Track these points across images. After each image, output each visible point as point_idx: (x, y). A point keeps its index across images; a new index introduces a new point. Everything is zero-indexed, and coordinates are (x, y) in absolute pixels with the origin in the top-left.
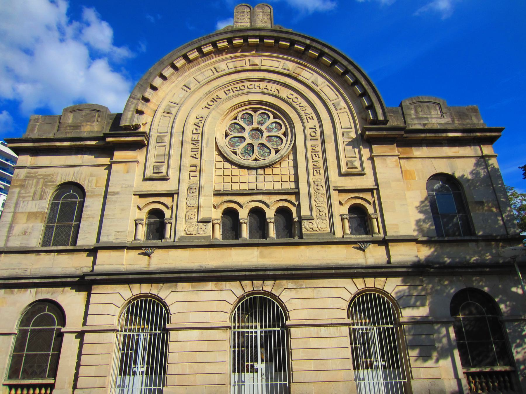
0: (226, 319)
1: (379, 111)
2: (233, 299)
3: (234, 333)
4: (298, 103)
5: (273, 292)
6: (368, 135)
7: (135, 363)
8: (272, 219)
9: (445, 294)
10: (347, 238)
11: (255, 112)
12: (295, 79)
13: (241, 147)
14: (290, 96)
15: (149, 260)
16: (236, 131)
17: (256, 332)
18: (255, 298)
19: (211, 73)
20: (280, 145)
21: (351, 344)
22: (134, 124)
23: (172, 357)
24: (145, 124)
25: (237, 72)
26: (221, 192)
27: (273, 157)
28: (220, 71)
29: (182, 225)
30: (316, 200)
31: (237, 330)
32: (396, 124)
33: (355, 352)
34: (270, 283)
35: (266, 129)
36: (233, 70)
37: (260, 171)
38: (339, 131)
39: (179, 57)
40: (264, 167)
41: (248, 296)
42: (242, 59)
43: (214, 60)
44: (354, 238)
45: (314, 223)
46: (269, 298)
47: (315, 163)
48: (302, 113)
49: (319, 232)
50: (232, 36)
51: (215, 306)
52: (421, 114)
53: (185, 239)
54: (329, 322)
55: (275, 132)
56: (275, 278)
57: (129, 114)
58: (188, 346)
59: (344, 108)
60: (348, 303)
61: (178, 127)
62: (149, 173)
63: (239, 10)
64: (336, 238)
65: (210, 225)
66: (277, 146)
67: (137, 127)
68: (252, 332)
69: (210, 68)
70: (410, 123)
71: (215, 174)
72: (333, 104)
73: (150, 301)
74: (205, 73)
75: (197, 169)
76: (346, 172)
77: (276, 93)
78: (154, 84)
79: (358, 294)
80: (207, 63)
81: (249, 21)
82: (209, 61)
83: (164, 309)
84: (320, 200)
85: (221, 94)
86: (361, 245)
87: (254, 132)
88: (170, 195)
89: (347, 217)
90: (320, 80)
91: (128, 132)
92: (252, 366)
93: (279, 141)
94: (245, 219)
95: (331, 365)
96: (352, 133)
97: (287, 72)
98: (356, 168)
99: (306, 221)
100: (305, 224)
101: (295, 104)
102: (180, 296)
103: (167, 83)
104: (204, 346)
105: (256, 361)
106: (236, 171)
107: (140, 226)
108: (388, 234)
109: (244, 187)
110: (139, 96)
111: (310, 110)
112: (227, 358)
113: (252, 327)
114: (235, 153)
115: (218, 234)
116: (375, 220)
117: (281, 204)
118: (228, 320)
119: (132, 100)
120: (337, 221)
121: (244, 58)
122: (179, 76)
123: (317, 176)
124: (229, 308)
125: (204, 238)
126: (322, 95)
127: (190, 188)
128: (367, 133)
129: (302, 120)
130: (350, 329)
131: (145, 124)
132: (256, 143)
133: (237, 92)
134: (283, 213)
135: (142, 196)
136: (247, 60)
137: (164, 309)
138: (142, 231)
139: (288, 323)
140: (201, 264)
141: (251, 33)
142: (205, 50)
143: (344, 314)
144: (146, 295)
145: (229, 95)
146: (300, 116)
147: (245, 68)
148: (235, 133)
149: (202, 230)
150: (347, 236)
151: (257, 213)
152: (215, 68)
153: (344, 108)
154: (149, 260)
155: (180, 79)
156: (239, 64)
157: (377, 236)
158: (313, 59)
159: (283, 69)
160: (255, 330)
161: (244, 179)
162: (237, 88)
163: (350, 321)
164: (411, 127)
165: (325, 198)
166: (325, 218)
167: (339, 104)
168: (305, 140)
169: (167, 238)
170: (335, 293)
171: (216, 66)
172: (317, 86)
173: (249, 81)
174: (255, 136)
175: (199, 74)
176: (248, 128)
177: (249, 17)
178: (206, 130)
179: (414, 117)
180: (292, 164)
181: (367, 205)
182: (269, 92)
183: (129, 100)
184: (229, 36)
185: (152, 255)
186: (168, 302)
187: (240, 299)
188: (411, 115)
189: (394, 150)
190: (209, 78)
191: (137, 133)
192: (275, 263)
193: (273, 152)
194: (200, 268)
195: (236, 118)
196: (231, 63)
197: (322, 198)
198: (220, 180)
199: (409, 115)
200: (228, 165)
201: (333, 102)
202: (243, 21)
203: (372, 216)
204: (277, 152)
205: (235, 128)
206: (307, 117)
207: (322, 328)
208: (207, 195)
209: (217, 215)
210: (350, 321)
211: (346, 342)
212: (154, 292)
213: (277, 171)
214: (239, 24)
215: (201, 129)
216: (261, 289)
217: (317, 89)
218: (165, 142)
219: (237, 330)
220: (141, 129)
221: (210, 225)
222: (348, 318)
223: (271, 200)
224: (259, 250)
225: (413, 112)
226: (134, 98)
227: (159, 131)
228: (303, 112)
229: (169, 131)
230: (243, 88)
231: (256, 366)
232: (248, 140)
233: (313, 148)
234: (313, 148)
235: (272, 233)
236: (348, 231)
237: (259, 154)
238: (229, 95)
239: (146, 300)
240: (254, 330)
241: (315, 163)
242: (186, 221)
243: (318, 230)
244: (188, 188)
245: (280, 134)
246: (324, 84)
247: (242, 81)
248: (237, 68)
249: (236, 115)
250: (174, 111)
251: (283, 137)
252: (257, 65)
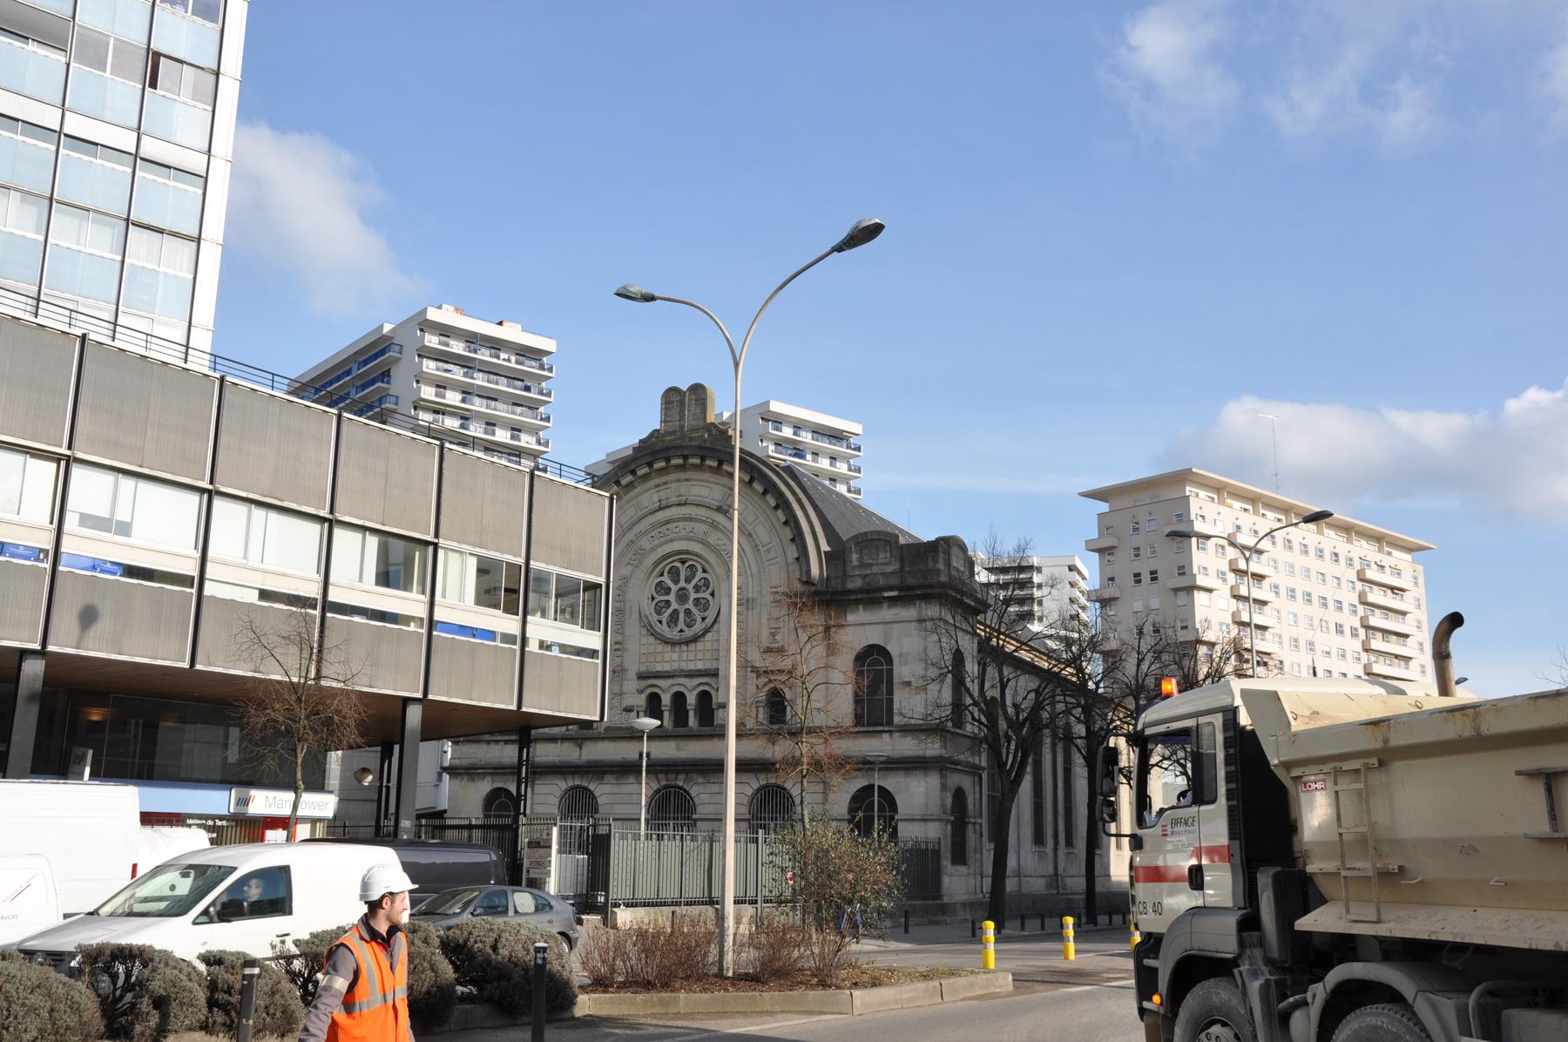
9: (1137, 938)
25: (661, 509)
52: (867, 560)
85: (645, 543)
106: (660, 648)
109: (667, 667)
117: (702, 688)
142: (624, 482)
151: (679, 698)
161: (667, 657)
184: (648, 459)
186: (597, 793)
213: (700, 645)
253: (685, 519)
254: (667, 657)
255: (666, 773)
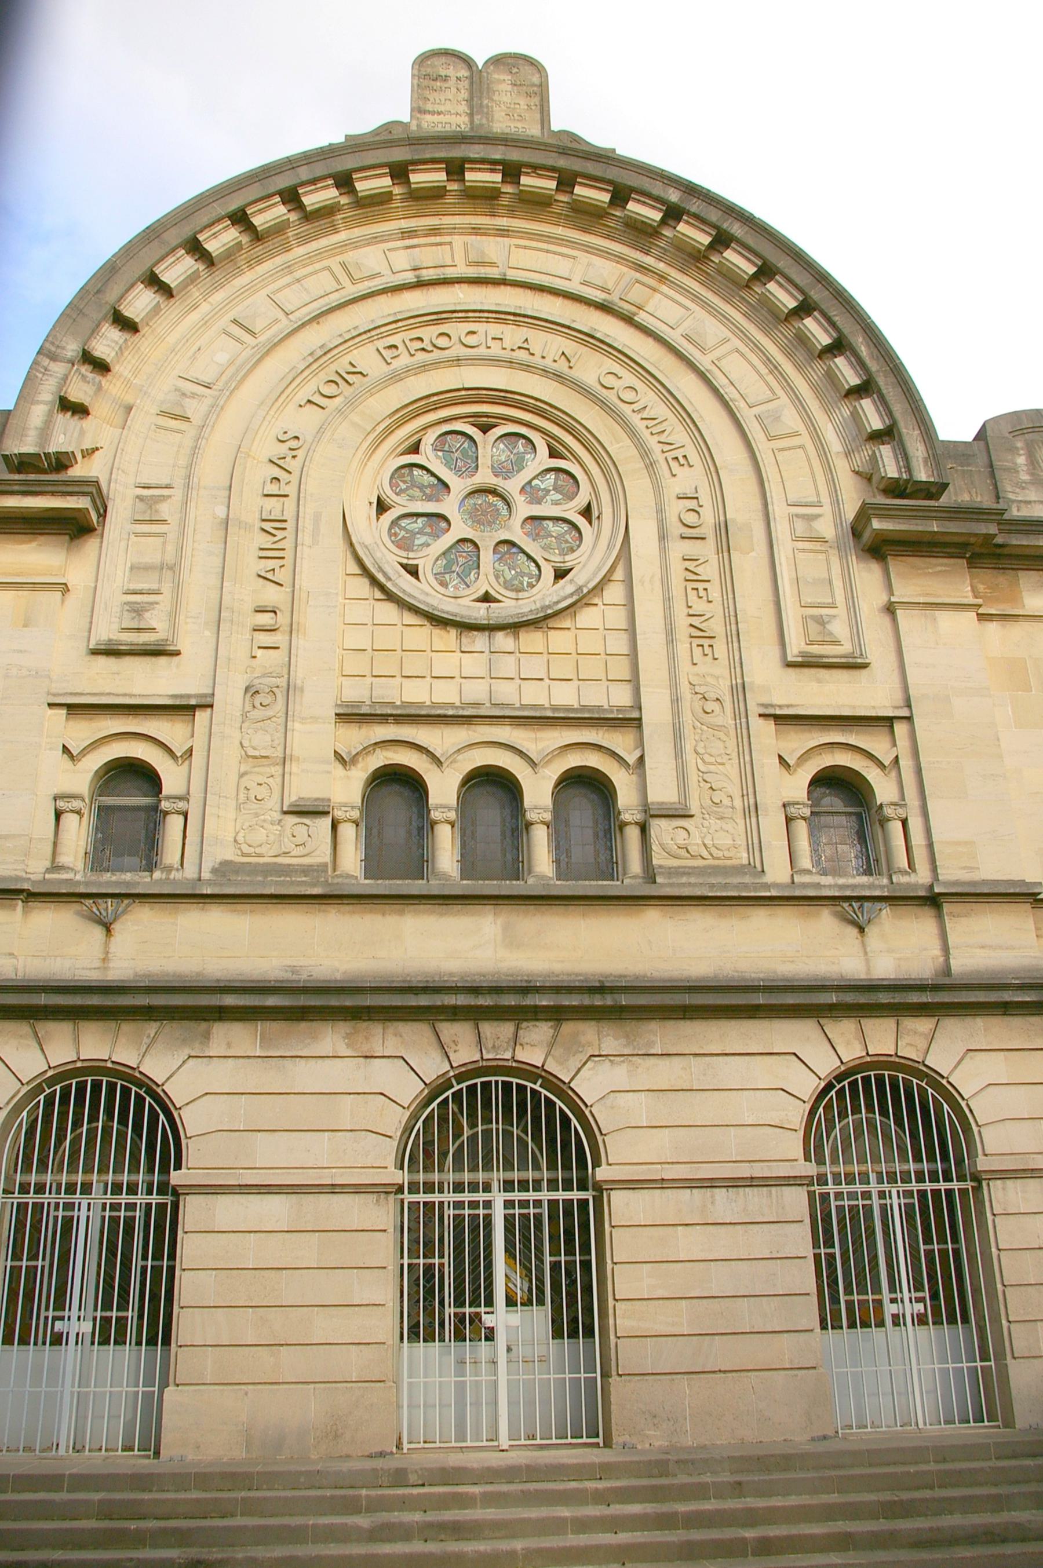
0: (380, 1160)
1: (917, 451)
2: (409, 1090)
3: (414, 1206)
4: (636, 407)
5: (551, 1067)
6: (878, 533)
7: (60, 1303)
8: (545, 810)
10: (804, 886)
11: (485, 429)
12: (629, 320)
13: (428, 555)
14: (609, 381)
15: (107, 944)
16: (417, 493)
17: (488, 1204)
18: (472, 1089)
19: (330, 284)
20: (573, 550)
21: (816, 1244)
22: (52, 449)
23: (189, 1286)
24: (88, 453)
25: (420, 284)
26: (365, 710)
27: (547, 593)
28: (362, 280)
29: (221, 821)
30: (701, 751)
31: (421, 1197)
32: (966, 497)
33: (826, 1272)
34: (539, 1032)
35: (523, 490)
36: (410, 277)
37: (503, 640)
38: (779, 510)
39: (219, 220)
40: (515, 627)
41: (460, 1078)
42: (438, 239)
43: (343, 236)
44: (829, 884)
45: (691, 829)
46: (537, 1087)
47: (696, 621)
48: (652, 442)
49: (711, 862)
50: (408, 157)
51: (347, 1111)
53: (237, 872)
54: (744, 1171)
55: (556, 503)
56: (557, 1015)
57: (38, 414)
58: (251, 1251)
59: (796, 434)
60: (808, 1106)
61: (211, 471)
62: (106, 631)
63: (429, 70)
64: (767, 886)
65: (327, 822)
66: (563, 554)
67: (61, 462)
68: (474, 1205)
69: (325, 263)
70: (1011, 496)
71: (346, 644)
72: (758, 417)
73: (112, 1087)
74: (308, 283)
75: (272, 624)
76: (803, 654)
77: (562, 366)
78: (129, 311)
79: (839, 1078)
80: (314, 245)
81: (463, 108)
82: (323, 242)
83: (162, 1117)
84: (714, 751)
85: (366, 358)
86: (854, 909)
87: (479, 500)
88: (183, 709)
89: (806, 811)
90: (712, 330)
91: (32, 477)
92: (476, 1318)
93: (571, 537)
94: (450, 809)
95: (747, 1315)
96: (821, 520)
97: (598, 296)
98: (836, 642)
99: (663, 823)
100: (660, 828)
101: (626, 409)
102: (219, 1075)
103: (172, 310)
104: (306, 1251)
105: (490, 1302)
107: (70, 821)
108: (944, 875)
109: (446, 695)
110: (72, 348)
111: (679, 435)
112: (382, 1292)
113: (474, 1187)
114: (413, 571)
115: (352, 860)
116: (896, 827)
118: (390, 1160)
119: (46, 362)
120: (772, 824)
121: (447, 239)
122: (217, 287)
123: (705, 666)
124: (395, 1120)
125: (306, 870)
126: (720, 381)
127: (252, 692)
128: (876, 524)
129: (650, 466)
130: (811, 1195)
131: (88, 453)
132: (487, 541)
133: (421, 356)
134: (585, 785)
135: (74, 709)
136: (462, 244)
137: (162, 1117)
138: (77, 834)
139: (602, 1173)
140: (289, 962)
141: (475, 151)
142: (312, 200)
143: (794, 1145)
144: (96, 1068)
145: (396, 364)
146: (644, 453)
147: (450, 273)
148: (412, 498)
149: (299, 840)
150: (806, 879)
151: (493, 784)
152: (343, 265)
153: (796, 434)
154: (107, 944)
155: (219, 296)
156: (431, 257)
157: (904, 879)
158: (690, 255)
159: (584, 283)
160: (486, 1196)
161: (445, 664)
162: (421, 339)
163: (811, 1169)
164: (1015, 513)
165: (732, 743)
166: (728, 813)
167: (778, 419)
168: (663, 537)
169: (169, 869)
170: (762, 1072)
171: (350, 257)
172: (703, 350)
173: (465, 320)
174: (485, 513)
175: (288, 285)
176: (459, 485)
177: (464, 94)
178: (311, 486)
179: (1025, 477)
180: (617, 618)
181: (872, 775)
182: (536, 360)
183: (35, 363)
185: (116, 927)
186: (177, 1092)
187: (436, 1089)
188: (1014, 470)
189: (955, 583)
190: (322, 302)
191: (66, 483)
192: (557, 967)
193: (548, 573)
194: (288, 976)
195: (415, 449)
196: (403, 253)
197: (721, 745)
198: (357, 664)
199: (1008, 470)
200: (389, 612)
201: (756, 410)
202: (441, 108)
203: (889, 811)
204: (560, 574)
205: (414, 484)
206: (670, 455)
207: (720, 1194)
208: (315, 719)
209: (347, 790)
210: (811, 1169)
211: (799, 1240)
212: (126, 1055)
213: (559, 640)
214: (428, 117)
215: (294, 479)
216: (508, 1055)
217: (704, 362)
218: (164, 521)
219: (421, 1197)
220: (77, 471)
221: (327, 822)
222: (807, 1158)
223: (541, 745)
224: (500, 921)
225: (1021, 460)
226: (54, 358)
227: (145, 480)
228: (656, 438)
229: (179, 482)
230: (442, 342)
231: (488, 1320)
232: (460, 529)
233: (691, 565)
234: (691, 565)
235: (542, 860)
236: (805, 861)
237: (497, 577)
238: (396, 364)
239: (97, 1086)
240: (481, 1197)
241: (696, 621)
242: (238, 808)
243: (705, 854)
244: (247, 689)
245: (571, 511)
246: (727, 348)
247: (439, 317)
248: (424, 272)
249: (415, 438)
250: (195, 409)
251: (581, 522)
252: (492, 264)
253: (500, 316)
254: (445, 664)
255: (475, 1015)
